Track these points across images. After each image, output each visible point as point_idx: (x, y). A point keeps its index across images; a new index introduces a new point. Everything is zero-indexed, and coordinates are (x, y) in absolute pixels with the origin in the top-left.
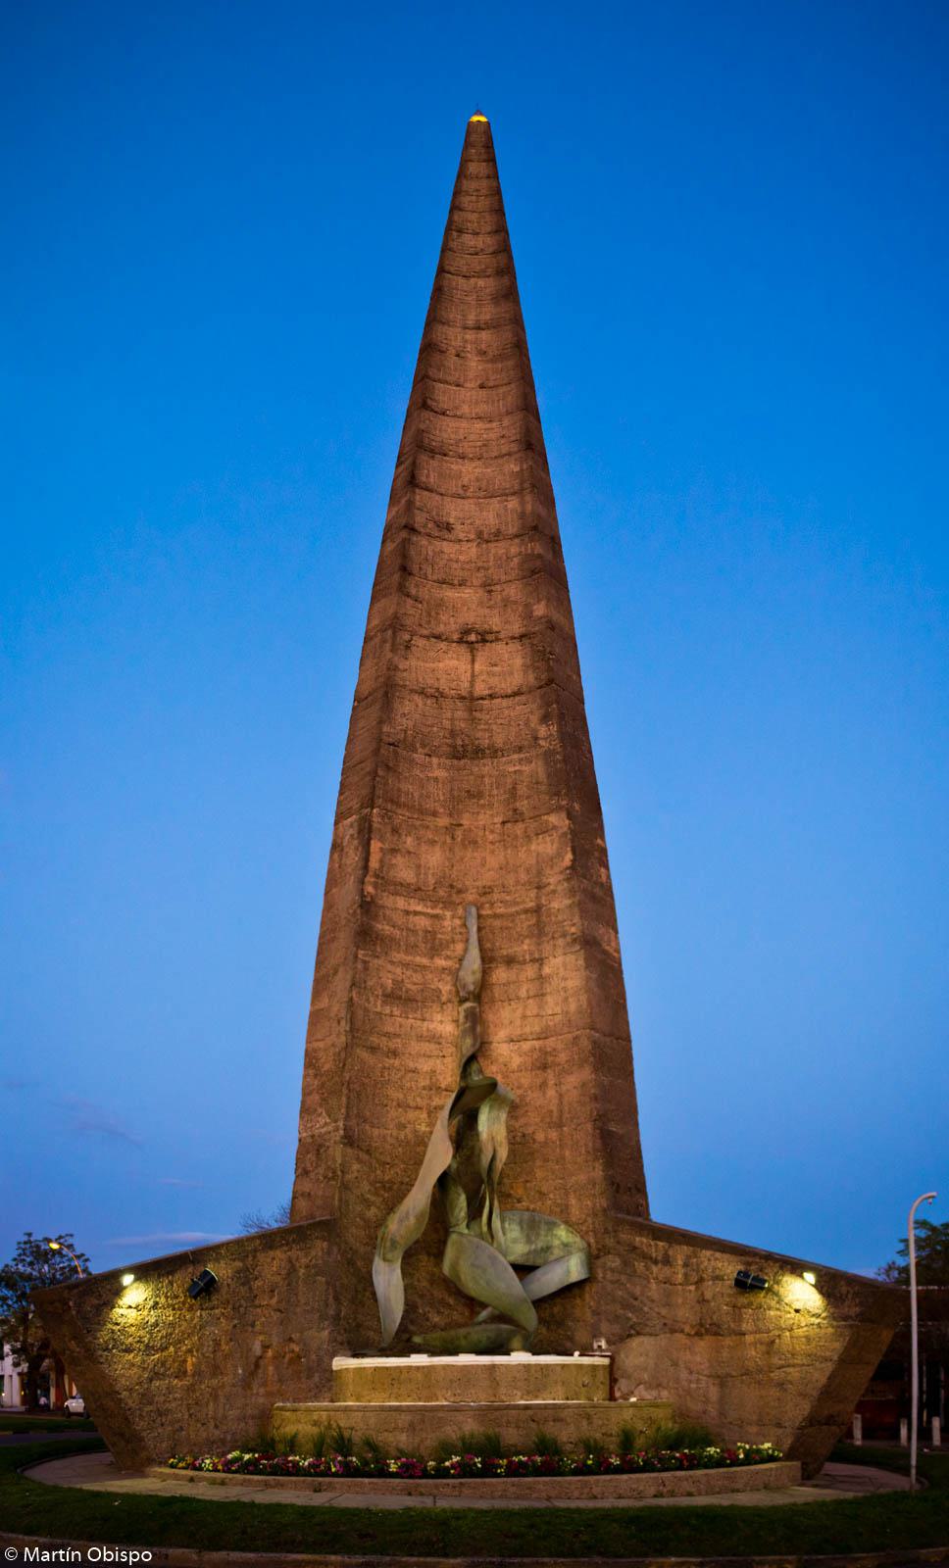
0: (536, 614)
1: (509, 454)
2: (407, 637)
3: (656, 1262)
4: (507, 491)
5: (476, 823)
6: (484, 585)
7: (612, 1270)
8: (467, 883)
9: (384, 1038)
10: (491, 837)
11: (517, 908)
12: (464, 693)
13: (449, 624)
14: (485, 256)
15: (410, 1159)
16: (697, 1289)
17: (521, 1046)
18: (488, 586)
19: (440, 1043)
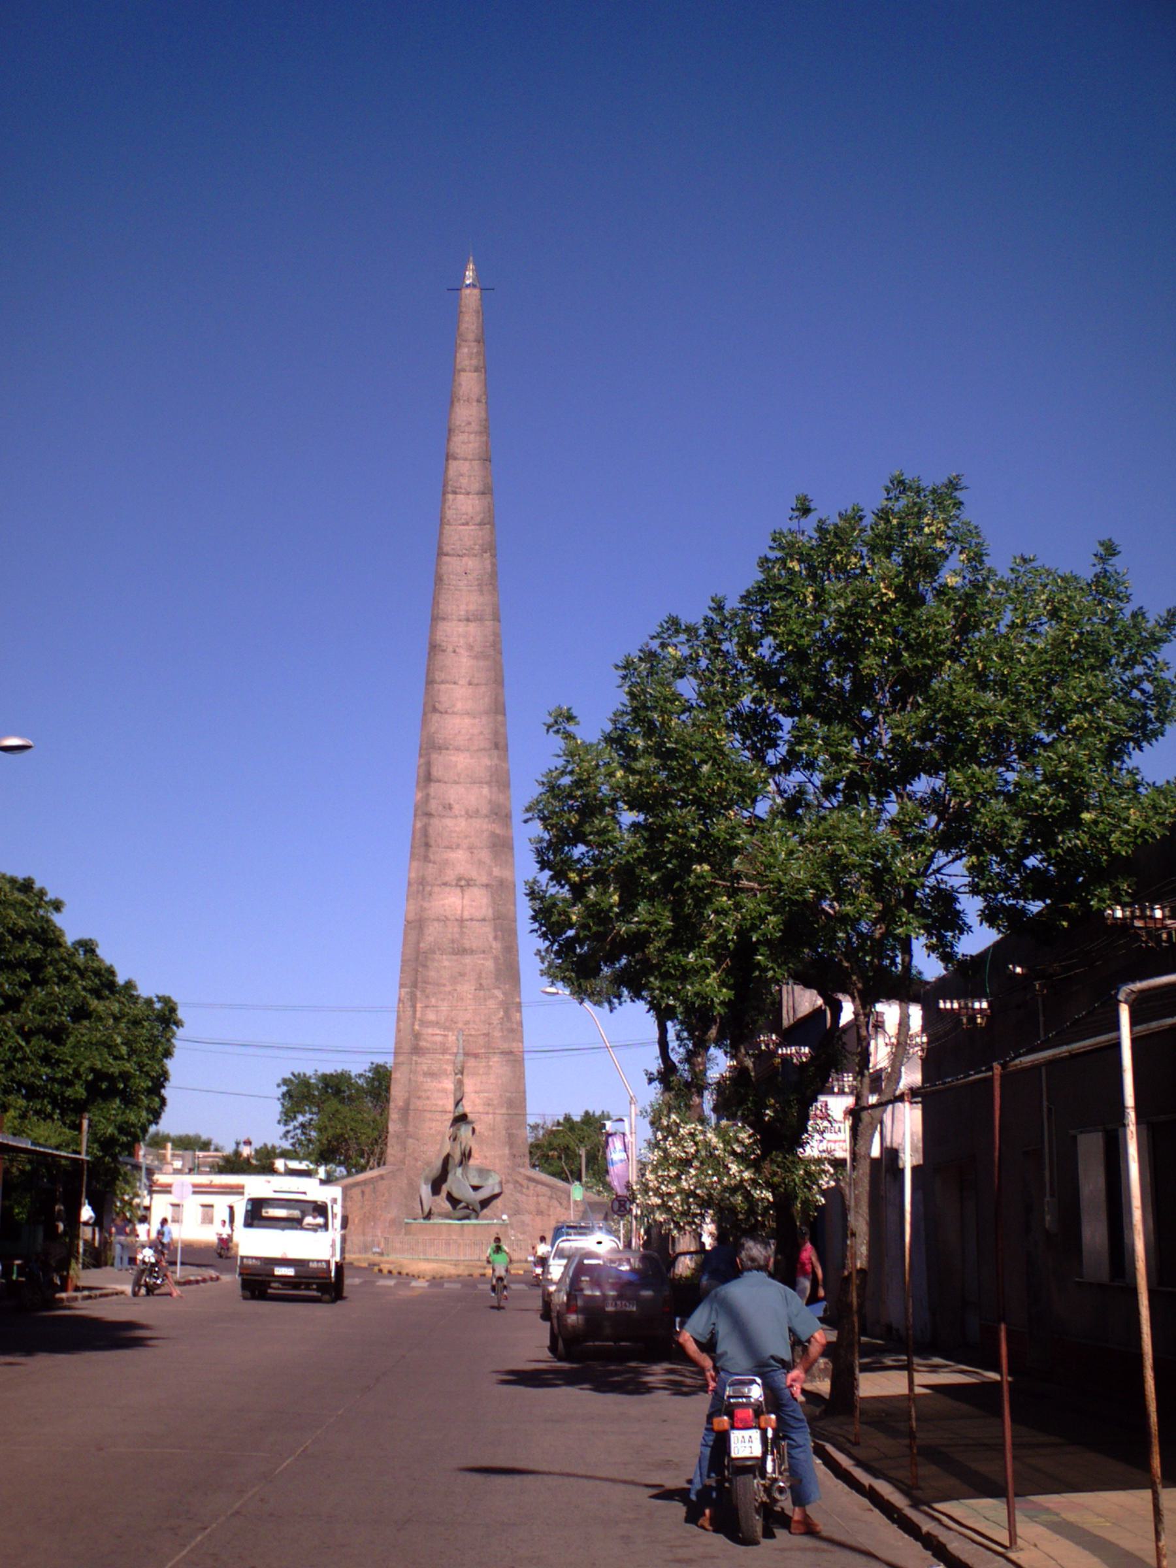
12: (458, 917)
13: (450, 876)
18: (471, 849)
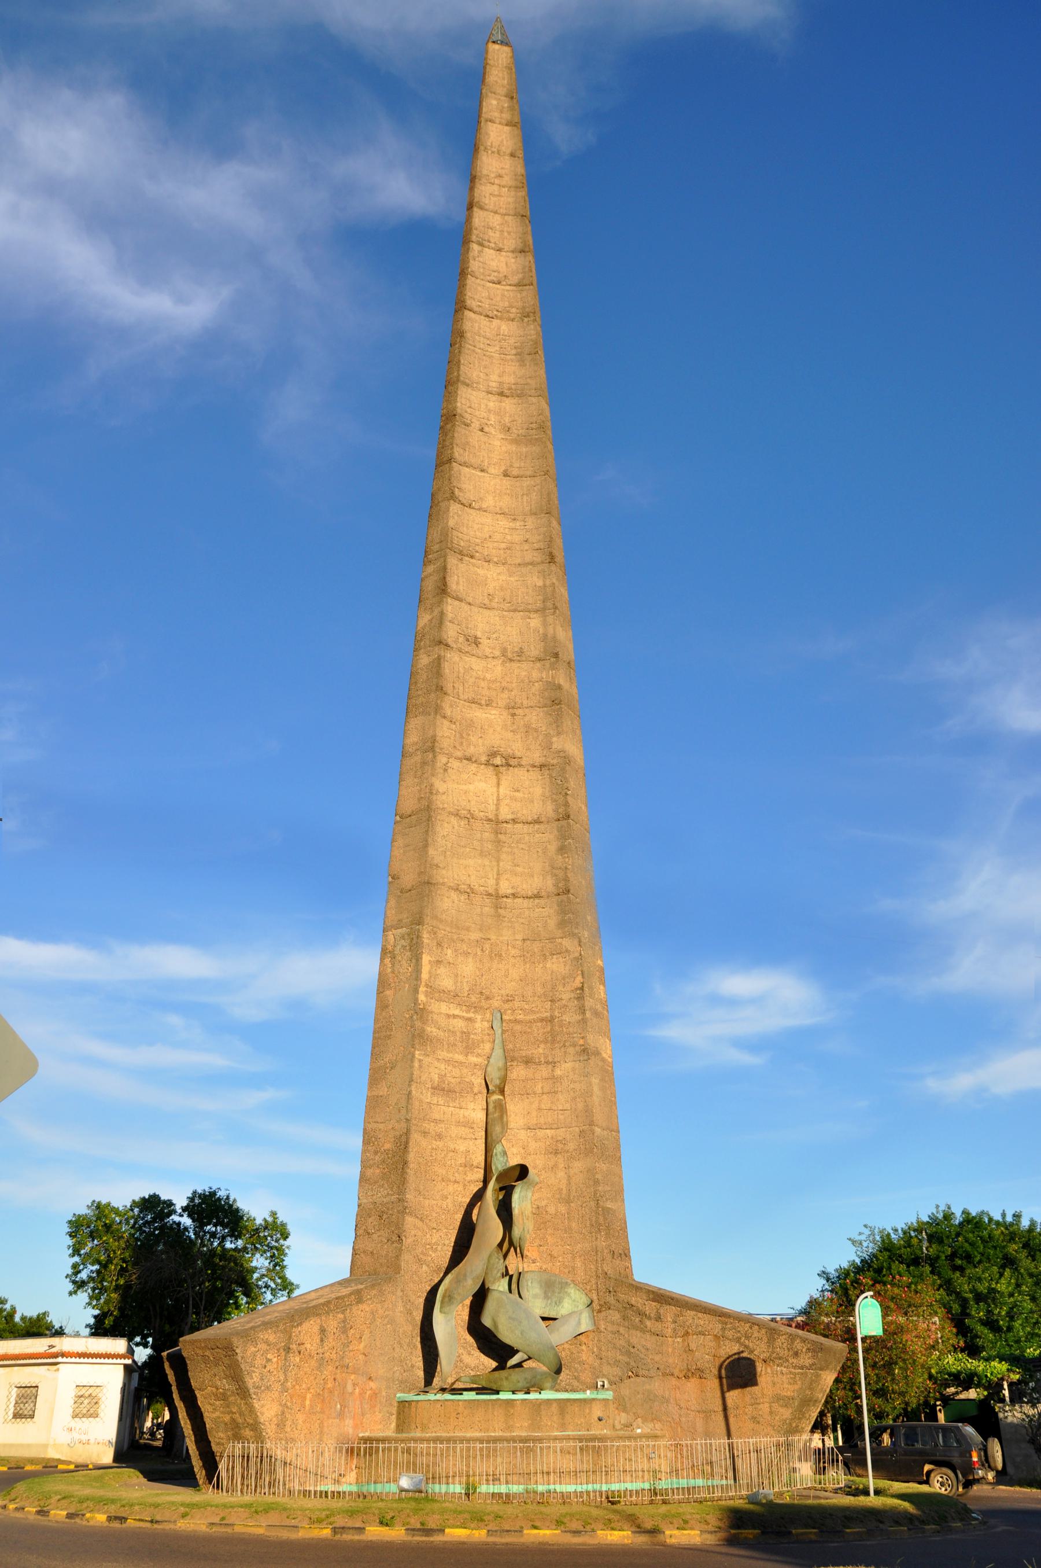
0: (554, 746)
1: (532, 564)
2: (444, 760)
3: (649, 1318)
4: (530, 607)
5: (501, 938)
6: (508, 707)
7: (613, 1323)
8: (493, 990)
9: (432, 1124)
10: (513, 952)
11: (535, 1017)
12: (491, 891)
13: (478, 747)
14: (508, 288)
15: (450, 1225)
16: (684, 1341)
17: (536, 1133)
18: (512, 708)
19: (472, 1128)
